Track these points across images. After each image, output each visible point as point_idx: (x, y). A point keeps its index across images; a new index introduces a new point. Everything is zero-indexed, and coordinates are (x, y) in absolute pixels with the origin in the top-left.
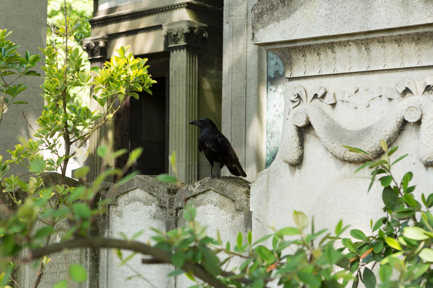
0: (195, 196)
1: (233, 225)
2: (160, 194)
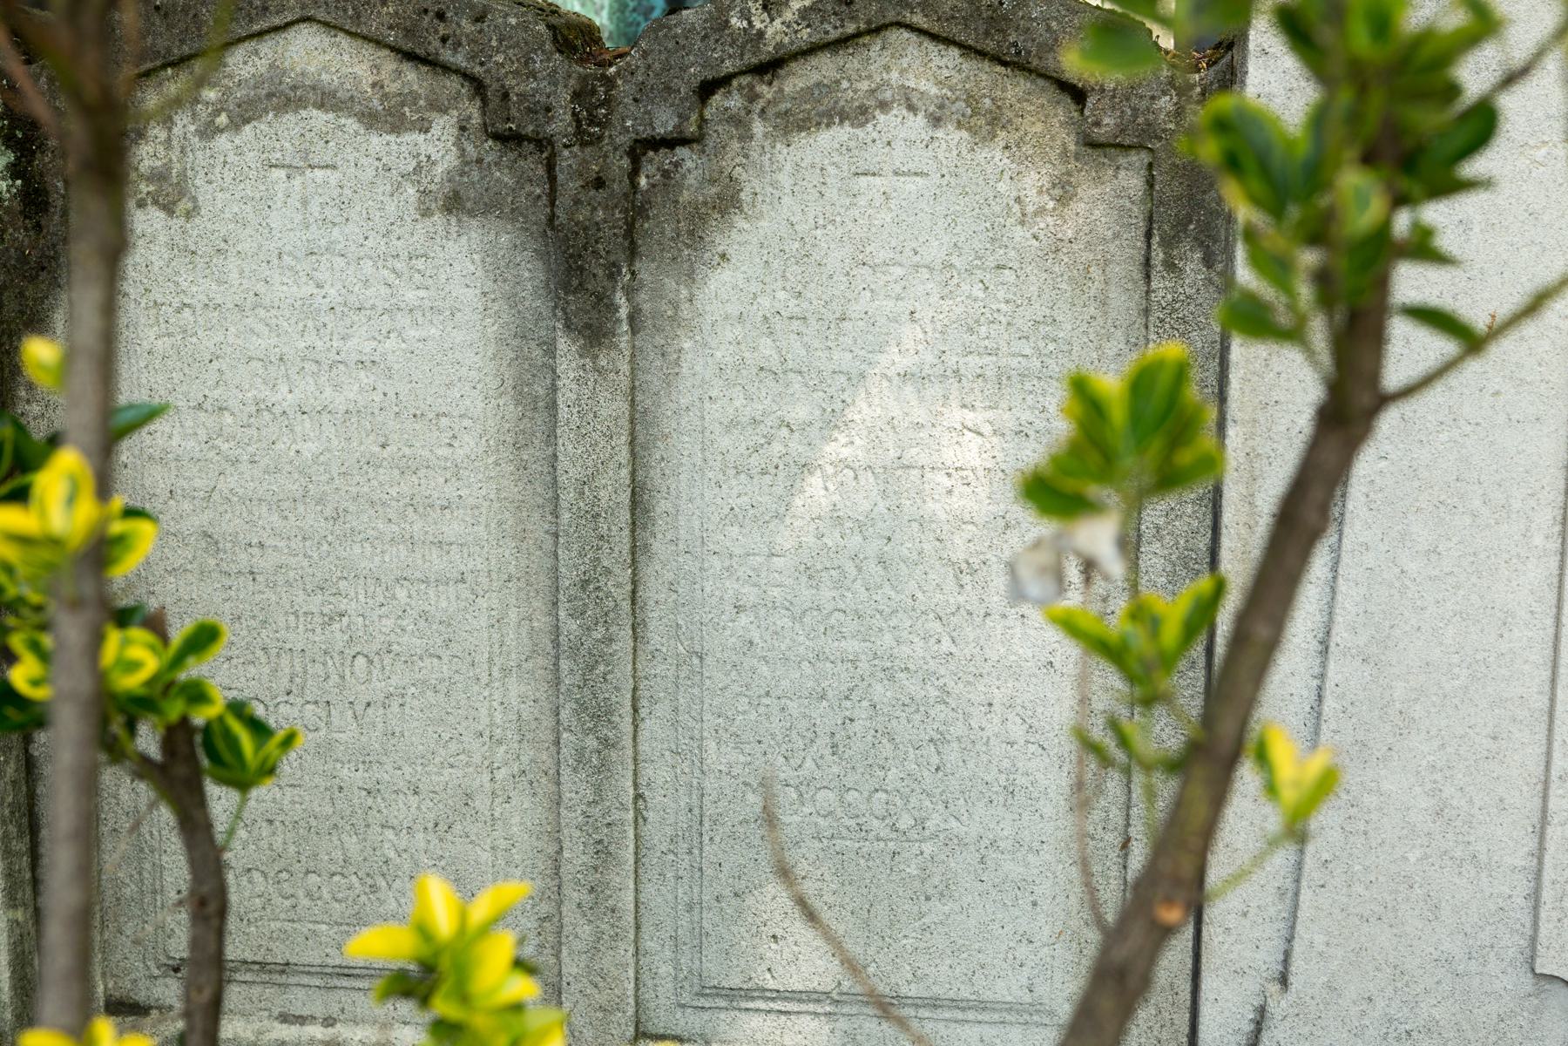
0: (770, 68)
1: (1070, 234)
2: (500, 58)
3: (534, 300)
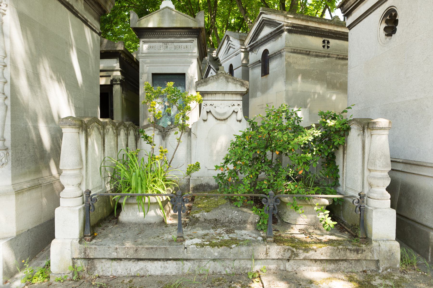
0: (172, 128)
3: (161, 139)
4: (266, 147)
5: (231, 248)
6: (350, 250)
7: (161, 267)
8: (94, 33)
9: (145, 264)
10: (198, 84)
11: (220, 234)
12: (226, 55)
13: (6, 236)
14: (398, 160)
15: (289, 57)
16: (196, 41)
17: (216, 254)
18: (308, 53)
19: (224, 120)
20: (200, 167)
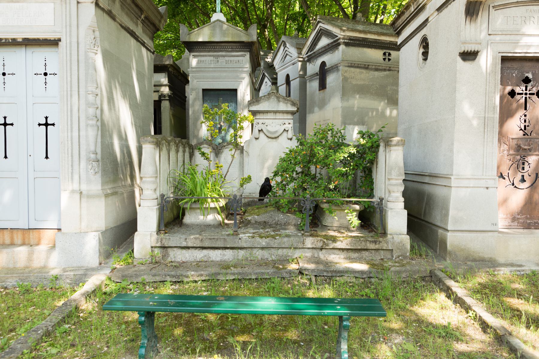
4: (309, 162)
5: (276, 239)
6: (370, 242)
7: (221, 254)
8: (149, 52)
9: (208, 252)
10: (250, 103)
11: (267, 232)
12: (283, 63)
13: (98, 229)
14: (426, 174)
15: (346, 71)
16: (248, 55)
17: (264, 243)
18: (366, 67)
19: (276, 138)
20: (252, 179)
